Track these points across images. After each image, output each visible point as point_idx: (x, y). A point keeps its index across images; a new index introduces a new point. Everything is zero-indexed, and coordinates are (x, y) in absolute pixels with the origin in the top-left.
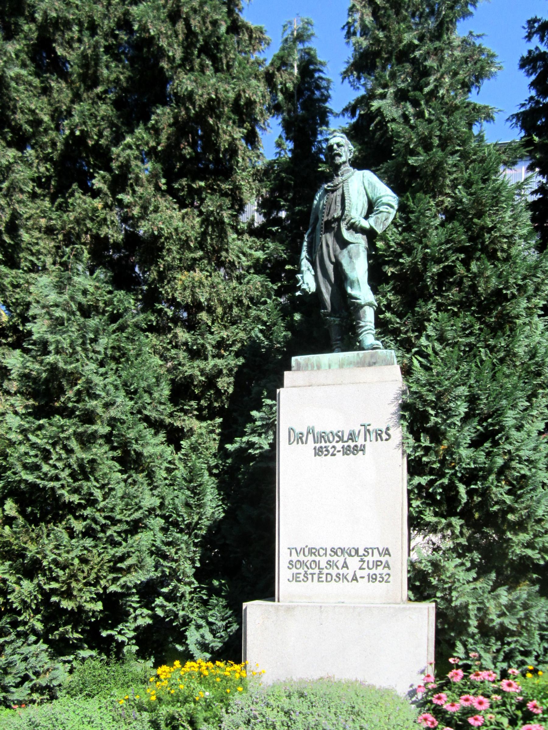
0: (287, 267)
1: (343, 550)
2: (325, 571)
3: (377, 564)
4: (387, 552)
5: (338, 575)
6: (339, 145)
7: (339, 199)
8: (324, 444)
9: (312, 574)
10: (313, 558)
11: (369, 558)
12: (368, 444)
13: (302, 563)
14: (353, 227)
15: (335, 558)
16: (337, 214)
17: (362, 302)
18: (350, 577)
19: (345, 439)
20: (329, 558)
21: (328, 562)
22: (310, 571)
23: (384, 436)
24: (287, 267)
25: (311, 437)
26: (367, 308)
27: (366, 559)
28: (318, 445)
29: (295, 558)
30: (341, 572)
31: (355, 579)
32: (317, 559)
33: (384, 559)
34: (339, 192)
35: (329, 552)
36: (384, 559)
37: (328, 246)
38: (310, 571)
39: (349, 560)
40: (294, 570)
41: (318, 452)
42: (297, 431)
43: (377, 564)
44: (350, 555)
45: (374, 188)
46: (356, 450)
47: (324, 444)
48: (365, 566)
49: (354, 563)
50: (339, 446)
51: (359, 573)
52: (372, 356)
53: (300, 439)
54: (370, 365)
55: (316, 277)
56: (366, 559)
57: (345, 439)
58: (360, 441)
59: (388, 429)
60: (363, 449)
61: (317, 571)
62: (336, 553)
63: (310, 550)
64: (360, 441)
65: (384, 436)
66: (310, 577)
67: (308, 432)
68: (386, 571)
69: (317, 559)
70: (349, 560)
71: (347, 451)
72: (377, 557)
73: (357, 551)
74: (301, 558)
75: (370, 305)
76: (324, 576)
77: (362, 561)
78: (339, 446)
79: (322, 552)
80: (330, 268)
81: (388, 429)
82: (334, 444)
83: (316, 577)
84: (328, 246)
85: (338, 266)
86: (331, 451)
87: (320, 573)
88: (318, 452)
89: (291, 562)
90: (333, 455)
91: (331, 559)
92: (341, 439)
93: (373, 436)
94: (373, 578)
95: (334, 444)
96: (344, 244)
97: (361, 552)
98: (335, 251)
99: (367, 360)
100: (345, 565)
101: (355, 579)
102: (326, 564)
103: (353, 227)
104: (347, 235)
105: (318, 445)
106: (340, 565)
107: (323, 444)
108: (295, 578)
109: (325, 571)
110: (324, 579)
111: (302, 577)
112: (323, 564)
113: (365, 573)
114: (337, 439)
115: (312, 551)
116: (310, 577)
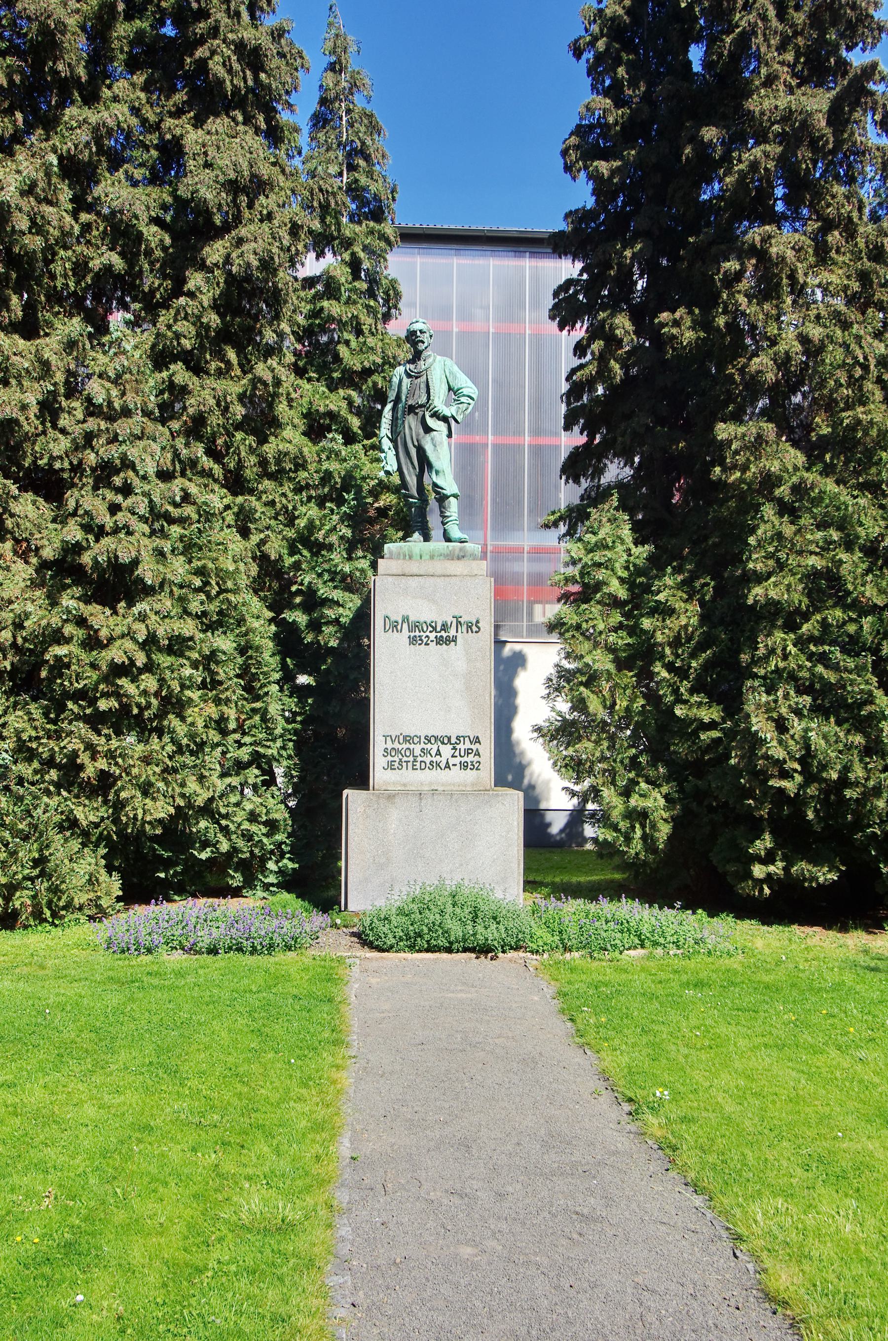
0: (825, 875)
1: (436, 738)
2: (419, 759)
3: (468, 752)
4: (477, 740)
5: (431, 763)
6: (421, 331)
7: (423, 386)
8: (418, 633)
9: (407, 762)
10: (408, 745)
11: (461, 746)
12: (459, 635)
13: (398, 751)
14: (435, 415)
15: (429, 746)
16: (423, 400)
17: (447, 492)
18: (443, 765)
19: (438, 629)
20: (423, 745)
21: (422, 750)
22: (405, 759)
23: (475, 629)
24: (825, 875)
25: (405, 626)
26: (452, 499)
27: (458, 747)
28: (412, 634)
29: (389, 745)
30: (434, 760)
31: (447, 766)
32: (412, 746)
33: (474, 747)
34: (423, 379)
35: (423, 739)
36: (474, 747)
37: (410, 428)
38: (405, 759)
39: (443, 748)
40: (390, 758)
41: (413, 641)
42: (393, 619)
43: (468, 752)
44: (443, 743)
45: (455, 377)
46: (449, 641)
47: (418, 633)
48: (457, 753)
49: (446, 750)
50: (432, 636)
51: (452, 761)
52: (461, 549)
53: (395, 626)
54: (458, 559)
55: (397, 455)
56: (458, 747)
57: (438, 629)
58: (452, 632)
59: (478, 622)
60: (454, 640)
61: (411, 759)
62: (430, 741)
63: (405, 737)
64: (452, 632)
65: (475, 629)
66: (404, 764)
67: (403, 621)
68: (477, 758)
69: (412, 746)
70: (443, 748)
71: (440, 641)
72: (468, 745)
73: (449, 739)
74: (396, 745)
75: (455, 496)
76: (418, 764)
77: (454, 748)
78: (432, 636)
79: (416, 740)
80: (413, 452)
81: (478, 622)
82: (428, 633)
83: (410, 765)
84: (410, 428)
85: (421, 451)
86: (425, 640)
87: (415, 761)
88: (413, 641)
89: (386, 750)
90: (427, 644)
91: (425, 747)
92: (435, 629)
93: (464, 628)
94: (464, 766)
95: (428, 633)
96: (428, 430)
97: (453, 740)
98: (418, 435)
99: (457, 552)
100: (438, 753)
101: (447, 766)
102: (413, 751)
103: (435, 415)
104: (431, 422)
105: (412, 634)
106: (433, 752)
107: (417, 634)
108: (390, 766)
109: (419, 759)
110: (418, 766)
111: (396, 764)
112: (417, 752)
113: (457, 760)
114: (430, 629)
115: (408, 739)
116: (404, 764)
